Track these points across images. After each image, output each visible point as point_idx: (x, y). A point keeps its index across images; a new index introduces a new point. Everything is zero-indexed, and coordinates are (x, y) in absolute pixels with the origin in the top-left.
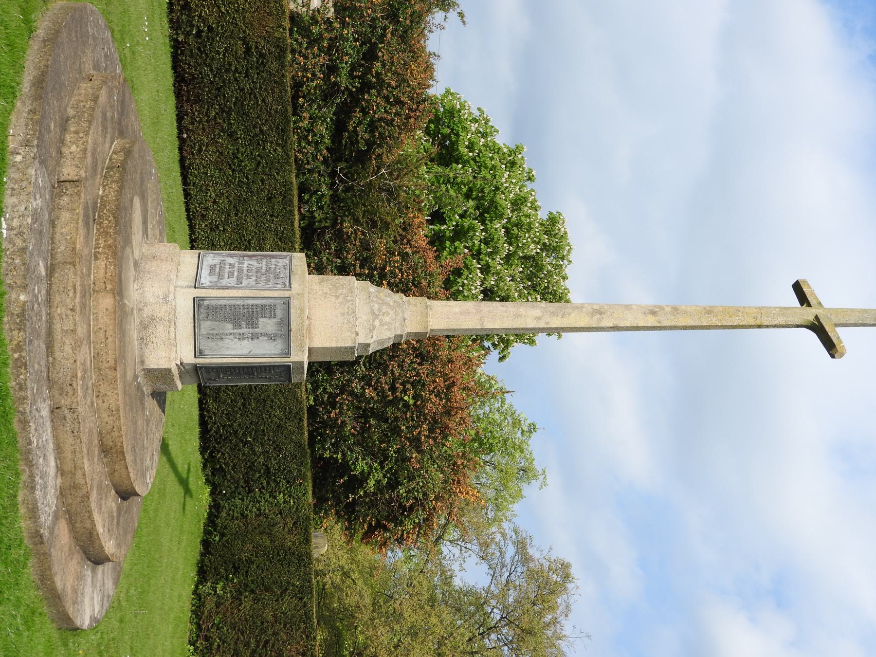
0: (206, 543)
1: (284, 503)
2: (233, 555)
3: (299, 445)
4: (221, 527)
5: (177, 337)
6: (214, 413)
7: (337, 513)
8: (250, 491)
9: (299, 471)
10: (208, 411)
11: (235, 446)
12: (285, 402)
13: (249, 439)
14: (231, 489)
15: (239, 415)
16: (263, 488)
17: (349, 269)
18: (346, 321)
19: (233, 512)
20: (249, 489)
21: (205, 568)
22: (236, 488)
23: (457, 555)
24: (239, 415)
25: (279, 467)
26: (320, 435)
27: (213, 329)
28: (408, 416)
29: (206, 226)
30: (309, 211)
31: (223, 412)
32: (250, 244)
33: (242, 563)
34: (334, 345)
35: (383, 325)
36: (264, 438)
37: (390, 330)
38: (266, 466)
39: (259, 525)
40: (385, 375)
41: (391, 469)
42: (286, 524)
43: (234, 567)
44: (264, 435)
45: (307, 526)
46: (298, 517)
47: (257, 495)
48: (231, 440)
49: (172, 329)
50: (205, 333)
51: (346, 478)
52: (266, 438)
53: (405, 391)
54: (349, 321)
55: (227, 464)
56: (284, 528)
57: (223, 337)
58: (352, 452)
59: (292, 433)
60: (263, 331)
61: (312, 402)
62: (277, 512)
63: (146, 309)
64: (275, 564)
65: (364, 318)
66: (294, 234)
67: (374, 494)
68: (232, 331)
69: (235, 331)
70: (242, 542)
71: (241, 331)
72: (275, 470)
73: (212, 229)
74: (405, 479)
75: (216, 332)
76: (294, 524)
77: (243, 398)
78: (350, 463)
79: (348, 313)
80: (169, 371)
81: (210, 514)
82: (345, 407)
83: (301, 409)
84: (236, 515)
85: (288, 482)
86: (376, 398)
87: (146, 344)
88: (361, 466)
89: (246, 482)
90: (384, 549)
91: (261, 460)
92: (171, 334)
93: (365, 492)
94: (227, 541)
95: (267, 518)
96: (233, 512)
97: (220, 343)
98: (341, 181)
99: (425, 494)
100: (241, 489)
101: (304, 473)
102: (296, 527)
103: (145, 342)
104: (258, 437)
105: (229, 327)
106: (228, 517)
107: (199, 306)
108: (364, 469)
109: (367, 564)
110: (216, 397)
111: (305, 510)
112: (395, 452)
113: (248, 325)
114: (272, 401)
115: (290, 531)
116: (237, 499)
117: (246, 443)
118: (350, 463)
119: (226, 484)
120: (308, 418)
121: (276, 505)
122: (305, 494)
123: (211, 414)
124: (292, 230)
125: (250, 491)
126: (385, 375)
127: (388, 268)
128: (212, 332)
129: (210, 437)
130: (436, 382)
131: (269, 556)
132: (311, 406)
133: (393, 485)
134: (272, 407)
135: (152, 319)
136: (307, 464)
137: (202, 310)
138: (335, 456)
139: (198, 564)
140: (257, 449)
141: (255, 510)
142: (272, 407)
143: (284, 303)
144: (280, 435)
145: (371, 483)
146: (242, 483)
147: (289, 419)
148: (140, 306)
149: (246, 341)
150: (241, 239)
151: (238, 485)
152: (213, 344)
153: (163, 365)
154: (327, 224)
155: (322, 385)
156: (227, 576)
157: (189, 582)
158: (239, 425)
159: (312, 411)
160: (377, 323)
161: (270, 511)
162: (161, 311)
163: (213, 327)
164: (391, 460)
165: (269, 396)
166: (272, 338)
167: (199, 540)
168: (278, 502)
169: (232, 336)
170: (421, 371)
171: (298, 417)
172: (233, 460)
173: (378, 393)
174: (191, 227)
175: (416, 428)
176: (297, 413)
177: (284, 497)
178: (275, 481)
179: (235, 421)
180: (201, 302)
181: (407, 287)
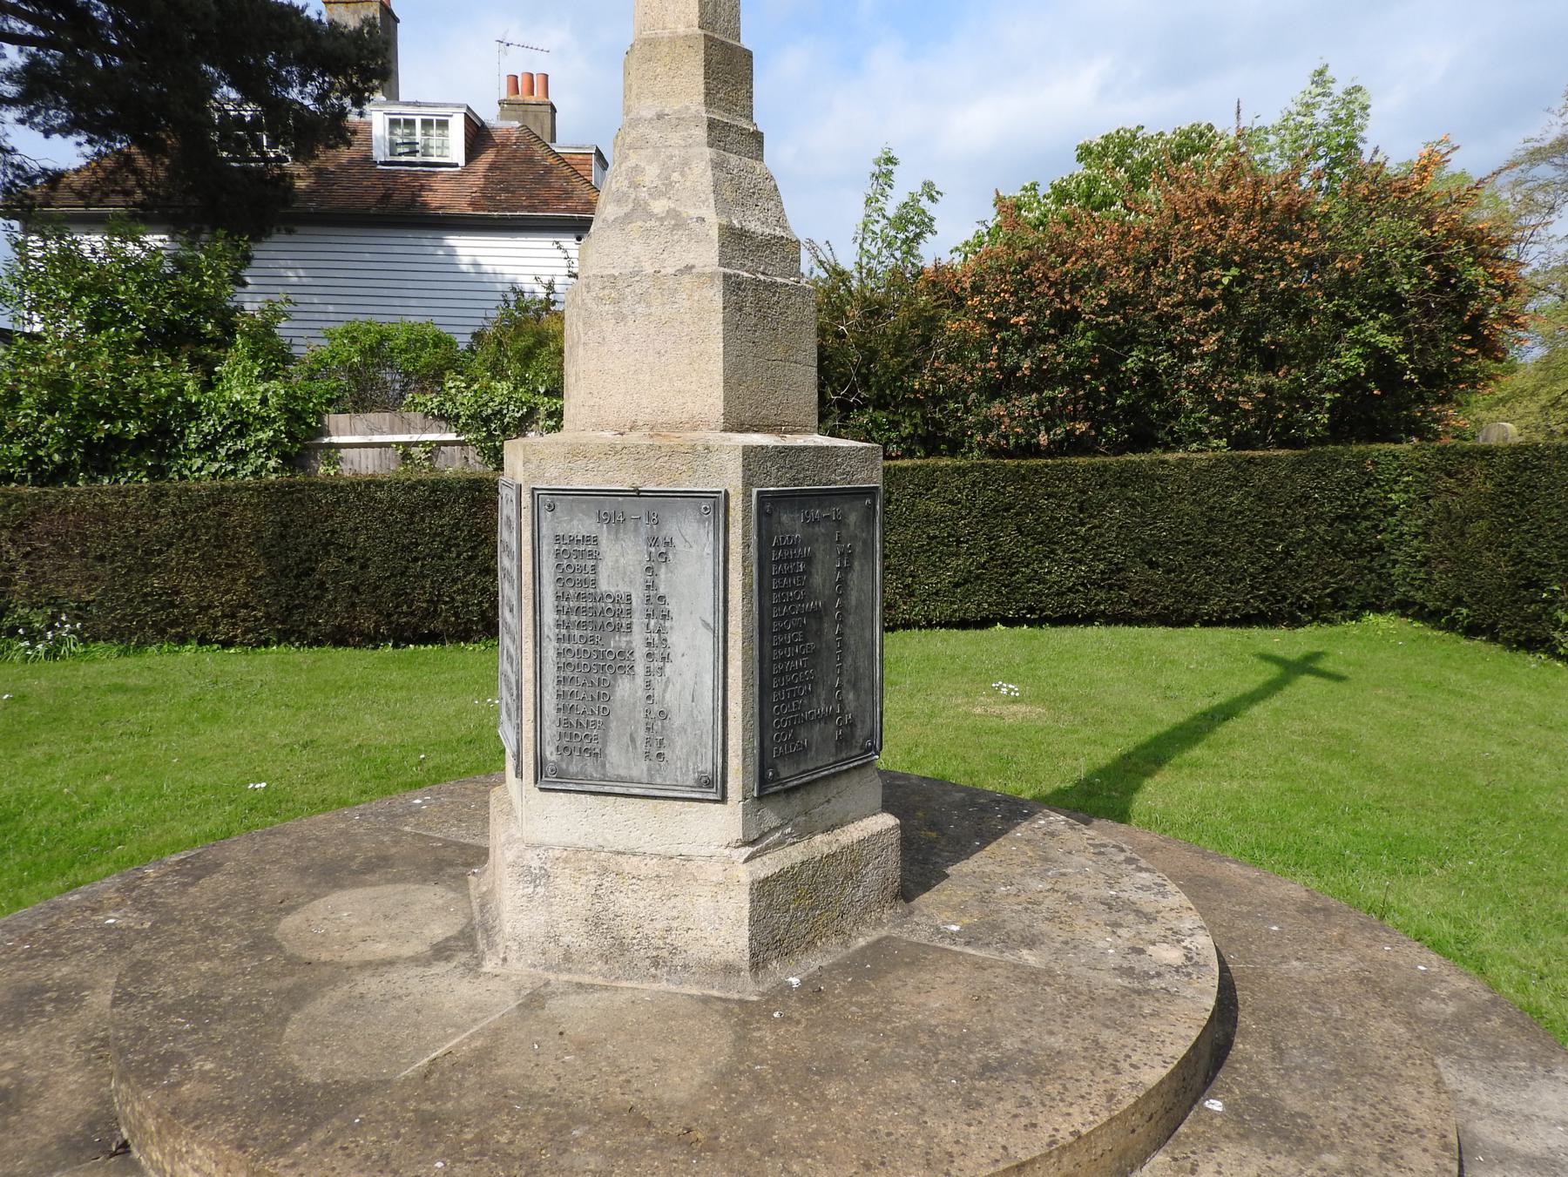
0: (1471, 631)
1: (1407, 492)
2: (1500, 587)
3: (1296, 466)
4: (1444, 601)
5: (661, 850)
6: (1228, 603)
7: (1441, 401)
8: (1380, 547)
9: (1348, 465)
10: (1224, 612)
11: (1291, 571)
12: (1215, 486)
13: (1279, 548)
14: (1372, 580)
15: (1235, 564)
16: (1375, 527)
17: (991, 379)
18: (640, 309)
19: (1415, 579)
20: (1376, 550)
21: (1522, 638)
22: (1371, 570)
23: (1542, 248)
24: (1235, 564)
25: (1338, 498)
26: (1286, 428)
27: (633, 740)
28: (1261, 277)
29: (905, 603)
30: (898, 444)
31: (1228, 589)
32: (935, 537)
33: (1519, 572)
34: (717, 347)
35: (670, 185)
36: (1280, 524)
37: (686, 163)
38: (1334, 520)
39: (1445, 537)
40: (1180, 317)
41: (1361, 307)
42: (1448, 490)
43: (1526, 587)
44: (1274, 523)
45: (1457, 453)
46: (1438, 468)
47: (1388, 537)
48: (1280, 578)
49: (628, 864)
50: (644, 765)
51: (1372, 385)
52: (1279, 520)
53: (1213, 284)
54: (642, 297)
55: (1326, 585)
56: (1456, 494)
57: (656, 708)
58: (1322, 375)
59: (1273, 476)
60: (640, 578)
61: (1223, 442)
62: (1424, 505)
63: (566, 939)
64: (1528, 512)
65: (637, 248)
66: (920, 467)
67: (1407, 333)
68: (640, 680)
69: (640, 669)
70: (1476, 568)
71: (640, 651)
72: (1342, 505)
73: (911, 595)
74: (1383, 282)
75: (642, 734)
76: (1450, 475)
77: (1204, 555)
78: (1342, 377)
79: (616, 302)
80: (762, 890)
81: (1417, 617)
82: (1236, 386)
83: (1231, 460)
84: (1422, 575)
85: (1368, 484)
86: (1221, 333)
87: (674, 951)
88: (1350, 358)
89: (1362, 554)
90: (1521, 320)
91: (1321, 529)
92: (644, 871)
93: (1402, 351)
94: (1472, 595)
95: (1433, 523)
96: (1415, 579)
97: (677, 720)
98: (852, 391)
99: (1418, 245)
100: (1375, 564)
101: (1353, 457)
102: (1457, 472)
103: (665, 953)
104: (1276, 534)
105: (627, 689)
106: (1425, 589)
107: (561, 774)
108: (1358, 354)
109: (1541, 374)
110: (1200, 599)
111: (1424, 455)
112: (1329, 301)
113: (617, 629)
114: (1212, 508)
115: (1465, 483)
116: (1392, 571)
117: (1287, 553)
118: (1342, 377)
119: (1362, 588)
120: (1254, 449)
121: (1410, 507)
122: (1394, 456)
123: (1229, 608)
124: (914, 469)
125: (1380, 547)
126: (1180, 317)
127: (990, 315)
128: (640, 741)
129: (1271, 610)
130: (1201, 231)
131: (1510, 524)
132: (1228, 444)
133: (1393, 302)
134: (1223, 509)
135: (595, 923)
136: (1336, 451)
137: (573, 769)
138: (1327, 405)
139: (1512, 650)
140: (1301, 536)
141: (1415, 543)
142: (1223, 509)
143: (552, 508)
144: (1276, 496)
145: (1384, 340)
146: (1361, 562)
147: (1248, 481)
148: (556, 953)
149: (673, 638)
150: (927, 551)
151: (1365, 568)
152: (679, 742)
153: (739, 905)
154: (919, 415)
155: (1194, 424)
156: (1544, 601)
157: (1548, 673)
158: (1253, 563)
159: (1238, 442)
160: (659, 206)
161: (1421, 517)
162: (574, 892)
163: (626, 739)
164: (1343, 305)
165: (1202, 514)
166: (660, 552)
167: (1464, 642)
168: (1404, 502)
169: (657, 681)
170: (1180, 257)
171: (1244, 465)
172: (1317, 574)
173: (1212, 330)
174: (907, 625)
175: (1285, 263)
176: (1237, 467)
177: (1395, 492)
178: (1363, 507)
179: (1245, 570)
180: (548, 769)
181: (1025, 282)
